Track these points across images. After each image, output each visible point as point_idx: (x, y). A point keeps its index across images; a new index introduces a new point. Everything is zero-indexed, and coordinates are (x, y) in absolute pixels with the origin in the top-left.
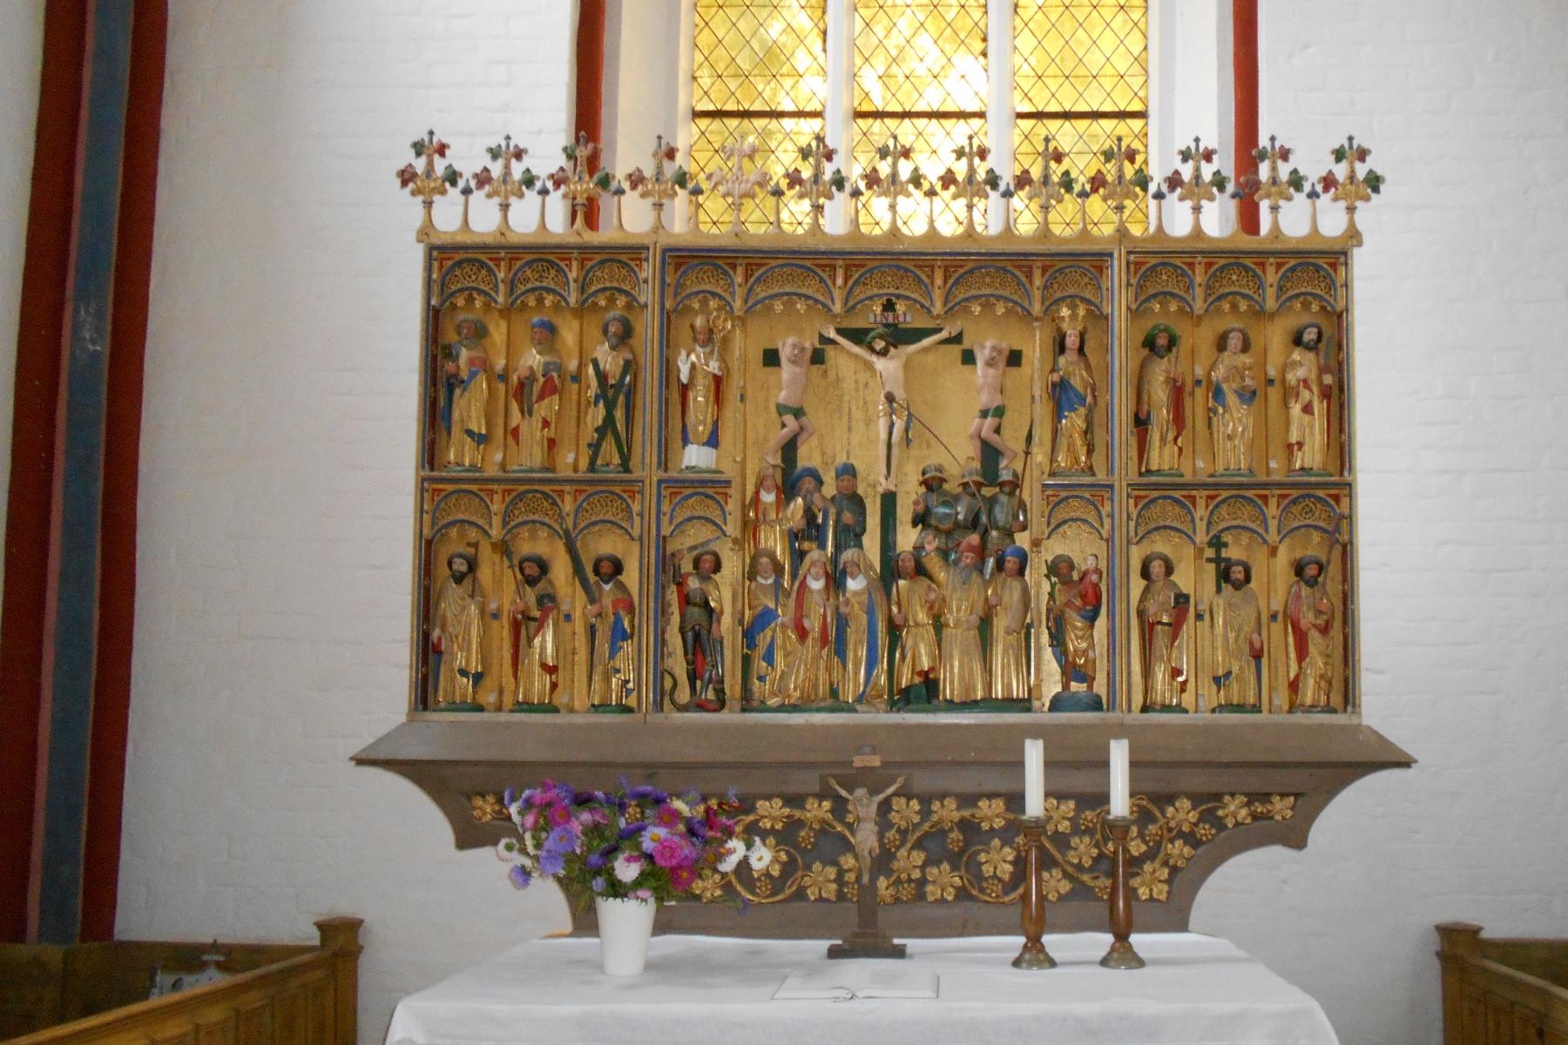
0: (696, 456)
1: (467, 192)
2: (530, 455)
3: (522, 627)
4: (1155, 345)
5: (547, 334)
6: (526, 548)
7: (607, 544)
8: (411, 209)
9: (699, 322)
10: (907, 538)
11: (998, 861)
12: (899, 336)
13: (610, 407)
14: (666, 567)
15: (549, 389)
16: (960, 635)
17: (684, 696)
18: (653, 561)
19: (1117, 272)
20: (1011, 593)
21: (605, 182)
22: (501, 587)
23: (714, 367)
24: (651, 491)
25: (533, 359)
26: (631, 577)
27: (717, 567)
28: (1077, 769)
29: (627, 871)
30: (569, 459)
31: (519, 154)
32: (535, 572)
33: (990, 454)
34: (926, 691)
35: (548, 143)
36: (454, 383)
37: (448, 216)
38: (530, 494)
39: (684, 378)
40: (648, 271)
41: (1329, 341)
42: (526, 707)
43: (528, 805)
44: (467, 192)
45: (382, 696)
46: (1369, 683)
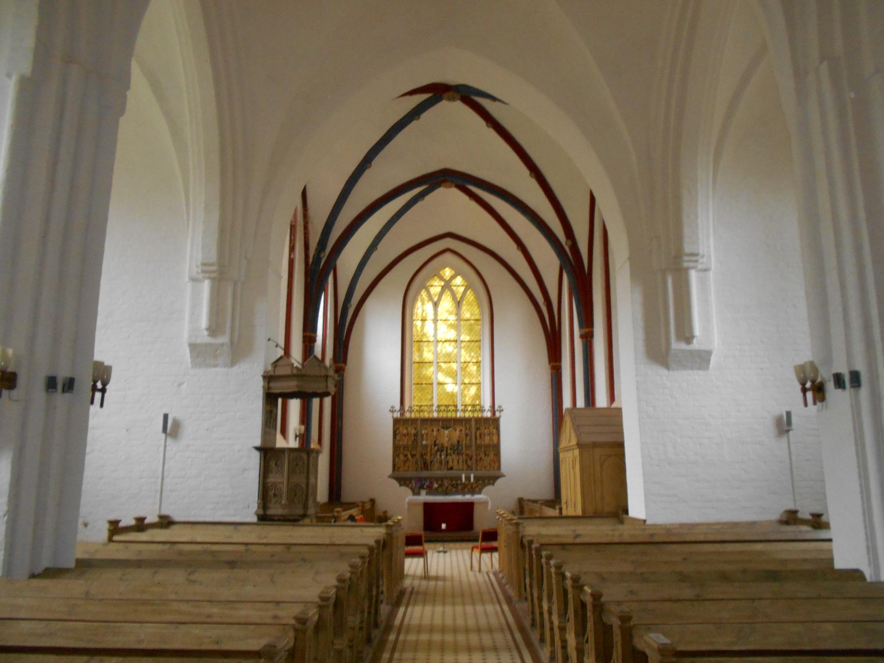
0: (424, 442)
2: (405, 442)
3: (405, 462)
4: (478, 429)
5: (407, 429)
7: (414, 453)
8: (390, 415)
10: (449, 451)
11: (460, 487)
12: (448, 428)
14: (422, 456)
16: (455, 462)
19: (473, 423)
20: (461, 457)
22: (402, 457)
25: (405, 431)
28: (468, 478)
30: (410, 443)
32: (406, 456)
33: (458, 442)
34: (451, 468)
35: (398, 407)
38: (406, 447)
41: (497, 428)
45: (389, 469)
46: (502, 467)
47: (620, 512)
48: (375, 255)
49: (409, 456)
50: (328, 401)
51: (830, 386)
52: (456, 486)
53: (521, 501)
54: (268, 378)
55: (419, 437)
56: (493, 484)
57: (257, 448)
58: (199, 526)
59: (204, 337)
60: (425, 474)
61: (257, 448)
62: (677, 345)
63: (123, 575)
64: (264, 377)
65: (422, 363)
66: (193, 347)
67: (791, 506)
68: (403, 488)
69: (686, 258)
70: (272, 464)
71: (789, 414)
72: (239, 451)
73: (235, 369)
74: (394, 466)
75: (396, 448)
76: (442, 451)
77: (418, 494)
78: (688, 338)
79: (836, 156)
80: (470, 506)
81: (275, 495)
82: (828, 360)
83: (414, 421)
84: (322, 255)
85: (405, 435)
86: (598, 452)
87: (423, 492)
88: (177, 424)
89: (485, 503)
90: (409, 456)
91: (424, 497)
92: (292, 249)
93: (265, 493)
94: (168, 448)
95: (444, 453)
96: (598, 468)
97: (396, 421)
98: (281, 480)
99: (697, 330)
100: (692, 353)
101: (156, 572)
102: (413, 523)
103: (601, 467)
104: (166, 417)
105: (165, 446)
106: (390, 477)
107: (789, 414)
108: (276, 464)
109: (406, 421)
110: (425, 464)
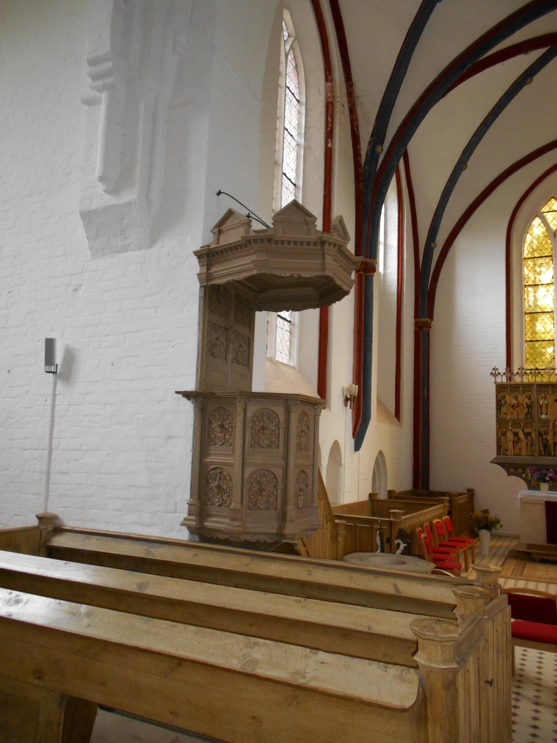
0: (543, 416)
1: (502, 376)
2: (515, 416)
5: (516, 398)
6: (514, 430)
7: (528, 430)
8: (493, 379)
9: (543, 395)
13: (529, 409)
14: (540, 434)
15: (518, 406)
17: (543, 454)
18: (217, 458)
21: (512, 374)
23: (546, 402)
24: (537, 422)
25: (514, 402)
26: (533, 435)
27: (548, 434)
29: (547, 479)
30: (522, 417)
31: (497, 369)
32: (516, 434)
35: (502, 368)
36: (501, 405)
37: (499, 379)
38: (515, 423)
39: (541, 404)
40: (534, 388)
42: (516, 455)
43: (530, 470)
44: (502, 376)
48: (464, 176)
49: (521, 435)
50: (343, 312)
54: (207, 256)
55: (535, 410)
57: (187, 395)
58: (94, 538)
59: (101, 199)
61: (187, 395)
64: (199, 255)
65: (534, 314)
66: (87, 216)
68: (512, 477)
72: (159, 402)
73: (155, 250)
74: (499, 447)
75: (501, 423)
77: (538, 488)
83: (527, 387)
84: (378, 149)
85: (513, 406)
87: (545, 486)
88: (70, 356)
90: (521, 435)
91: (545, 493)
92: (329, 135)
93: (206, 484)
94: (59, 399)
97: (500, 388)
104: (50, 344)
105: (54, 396)
109: (516, 387)
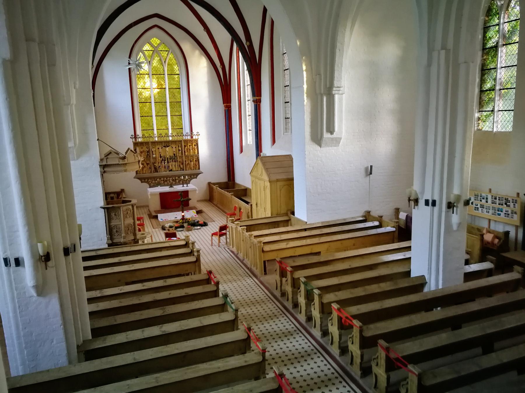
0: (154, 156)
7: (148, 162)
10: (169, 160)
33: (174, 154)
34: (171, 170)
47: (289, 213)
51: (422, 202)
52: (177, 180)
53: (209, 184)
56: (196, 178)
60: (156, 174)
62: (326, 135)
63: (127, 335)
67: (367, 209)
69: (334, 89)
70: (113, 214)
71: (371, 167)
76: (165, 160)
78: (331, 130)
79: (441, 102)
80: (186, 193)
81: (117, 231)
82: (423, 192)
86: (279, 184)
89: (195, 190)
95: (166, 162)
96: (279, 192)
98: (120, 223)
99: (336, 129)
100: (332, 139)
101: (143, 331)
102: (155, 204)
103: (280, 191)
106: (135, 178)
107: (371, 167)
108: (115, 215)
110: (155, 168)
